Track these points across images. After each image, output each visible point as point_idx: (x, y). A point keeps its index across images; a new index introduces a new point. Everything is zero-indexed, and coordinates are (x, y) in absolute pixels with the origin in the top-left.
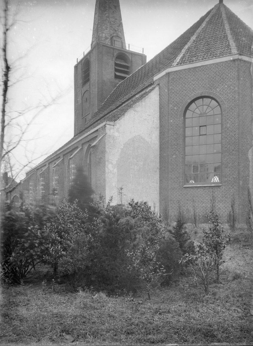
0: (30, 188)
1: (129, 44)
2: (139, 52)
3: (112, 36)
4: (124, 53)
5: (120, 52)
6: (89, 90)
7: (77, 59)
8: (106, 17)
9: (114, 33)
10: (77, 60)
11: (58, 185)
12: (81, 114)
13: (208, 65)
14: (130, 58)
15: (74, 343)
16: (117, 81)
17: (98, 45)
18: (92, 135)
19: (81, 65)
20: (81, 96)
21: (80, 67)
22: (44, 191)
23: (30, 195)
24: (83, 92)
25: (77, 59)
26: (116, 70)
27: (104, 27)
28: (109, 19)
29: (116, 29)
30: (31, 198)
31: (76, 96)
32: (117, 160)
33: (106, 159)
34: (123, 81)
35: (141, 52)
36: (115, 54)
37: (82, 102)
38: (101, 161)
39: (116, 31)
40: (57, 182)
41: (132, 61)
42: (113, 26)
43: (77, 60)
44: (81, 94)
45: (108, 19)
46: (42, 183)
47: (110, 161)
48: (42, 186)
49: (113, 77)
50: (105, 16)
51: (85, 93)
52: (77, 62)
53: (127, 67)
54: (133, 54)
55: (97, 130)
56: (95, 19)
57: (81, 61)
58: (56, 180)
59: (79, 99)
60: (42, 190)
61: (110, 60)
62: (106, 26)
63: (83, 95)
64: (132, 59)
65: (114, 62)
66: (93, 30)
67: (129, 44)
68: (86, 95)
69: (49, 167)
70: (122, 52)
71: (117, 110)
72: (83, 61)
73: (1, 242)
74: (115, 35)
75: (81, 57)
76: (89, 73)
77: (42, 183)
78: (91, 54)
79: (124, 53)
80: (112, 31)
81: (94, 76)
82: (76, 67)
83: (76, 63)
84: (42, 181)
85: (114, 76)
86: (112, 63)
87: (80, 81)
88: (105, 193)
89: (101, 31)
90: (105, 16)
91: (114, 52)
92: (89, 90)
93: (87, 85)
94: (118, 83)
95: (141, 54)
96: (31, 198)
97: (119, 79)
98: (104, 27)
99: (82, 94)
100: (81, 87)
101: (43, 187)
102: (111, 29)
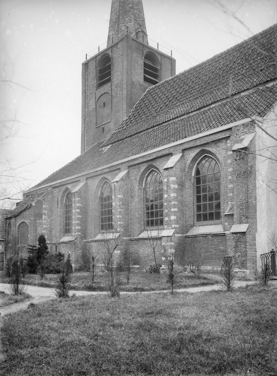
0: (44, 212)
1: (158, 43)
2: (167, 54)
3: (137, 31)
4: (154, 54)
5: (149, 50)
6: (110, 92)
7: (86, 54)
8: (129, 7)
9: (139, 28)
10: (86, 56)
11: (122, 206)
12: (95, 121)
14: (160, 60)
16: (146, 84)
18: (212, 137)
20: (94, 100)
21: (92, 66)
22: (80, 216)
23: (44, 222)
24: (98, 95)
25: (86, 54)
26: (145, 72)
27: (126, 19)
28: (134, 10)
29: (141, 24)
30: (44, 226)
31: (85, 100)
32: (266, 170)
33: (257, 169)
34: (154, 86)
35: (170, 55)
36: (145, 52)
37: (96, 107)
38: (252, 171)
39: (141, 26)
40: (121, 203)
41: (161, 64)
42: (137, 19)
43: (86, 56)
45: (132, 10)
46: (77, 205)
47: (260, 171)
48: (78, 208)
49: (142, 80)
50: (129, 6)
51: (102, 97)
52: (86, 58)
55: (230, 129)
56: (113, 9)
57: (96, 57)
58: (120, 200)
59: (92, 104)
60: (79, 214)
61: (139, 59)
62: (129, 18)
64: (161, 62)
65: (143, 61)
66: (110, 22)
67: (158, 43)
68: (104, 99)
69: (86, 183)
70: (152, 51)
71: (198, 112)
72: (99, 57)
74: (140, 30)
77: (77, 205)
79: (154, 52)
80: (137, 25)
82: (86, 65)
84: (78, 203)
86: (141, 62)
87: (93, 82)
88: (256, 216)
89: (123, 23)
90: (129, 6)
91: (144, 49)
92: (110, 92)
93: (106, 88)
94: (147, 88)
95: (170, 56)
96: (45, 226)
97: (148, 83)
98: (126, 19)
99: (96, 98)
100: (95, 88)
101: (79, 210)
102: (136, 23)
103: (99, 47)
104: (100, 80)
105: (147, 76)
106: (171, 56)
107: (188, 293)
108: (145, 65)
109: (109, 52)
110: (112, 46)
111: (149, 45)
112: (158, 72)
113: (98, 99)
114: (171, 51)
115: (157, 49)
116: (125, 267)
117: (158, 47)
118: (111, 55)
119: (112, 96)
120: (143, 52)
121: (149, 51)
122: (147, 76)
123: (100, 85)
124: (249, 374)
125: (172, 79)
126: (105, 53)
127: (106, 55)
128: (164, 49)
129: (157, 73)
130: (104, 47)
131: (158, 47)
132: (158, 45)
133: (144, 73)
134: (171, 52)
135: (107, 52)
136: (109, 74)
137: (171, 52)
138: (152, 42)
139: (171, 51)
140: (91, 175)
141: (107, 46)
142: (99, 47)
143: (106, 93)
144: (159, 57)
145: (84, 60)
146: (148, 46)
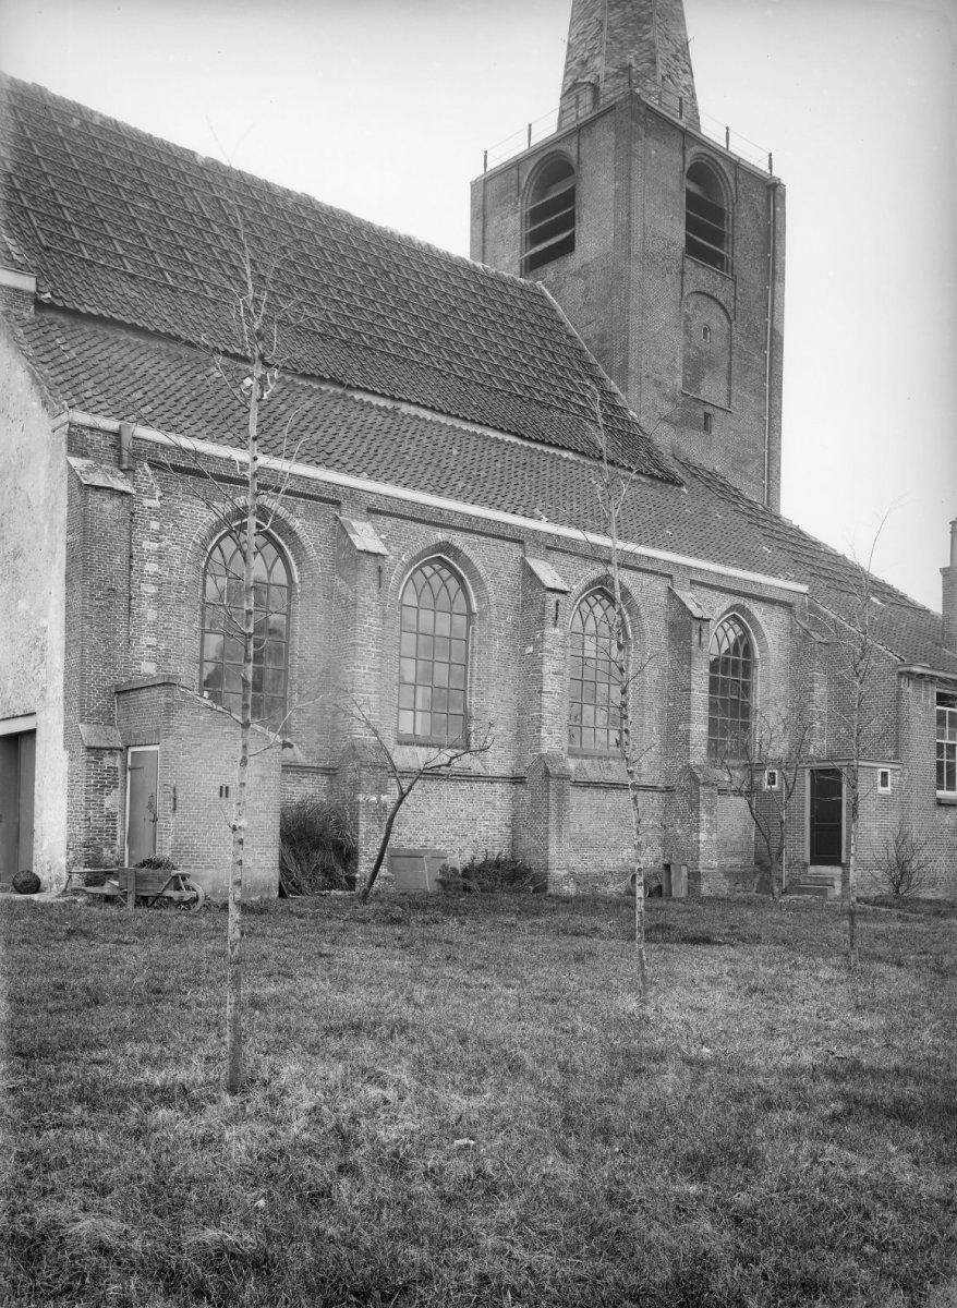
35: (765, 168)
57: (517, 164)
95: (765, 172)
104: (533, 223)
105: (691, 235)
106: (768, 172)
107: (560, 458)
109: (571, 149)
110: (576, 131)
111: (703, 131)
112: (726, 244)
115: (725, 146)
118: (574, 154)
122: (691, 235)
128: (749, 149)
129: (722, 249)
130: (546, 127)
132: (727, 133)
133: (688, 207)
135: (563, 147)
136: (569, 221)
138: (711, 129)
140: (708, 581)
141: (559, 128)
145: (478, 172)
146: (698, 135)
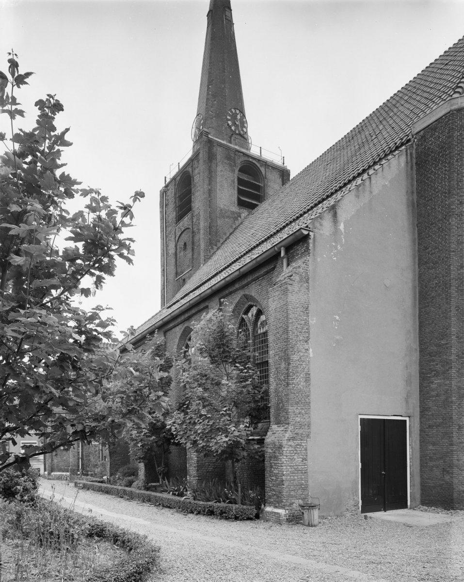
1: (261, 148)
5: (246, 159)
13: (442, 117)
14: (263, 172)
15: (295, 557)
17: (206, 146)
19: (173, 188)
21: (171, 193)
26: (240, 192)
37: (176, 252)
44: (173, 236)
53: (258, 188)
54: (266, 164)
57: (174, 179)
63: (178, 239)
64: (266, 176)
67: (261, 148)
68: (185, 237)
72: (179, 177)
73: (134, 255)
75: (172, 171)
76: (191, 197)
78: (195, 162)
79: (254, 161)
81: (198, 203)
83: (164, 185)
85: (236, 202)
87: (172, 215)
92: (190, 227)
93: (186, 221)
103: (179, 163)
108: (241, 182)
113: (179, 237)
114: (284, 157)
116: (97, 443)
117: (261, 153)
119: (193, 232)
120: (235, 162)
121: (245, 161)
123: (180, 218)
124: (62, 581)
125: (419, 245)
126: (185, 170)
127: (260, 175)
129: (260, 193)
131: (261, 153)
134: (283, 159)
135: (187, 169)
137: (283, 159)
139: (284, 157)
142: (179, 163)
143: (186, 229)
144: (262, 169)
